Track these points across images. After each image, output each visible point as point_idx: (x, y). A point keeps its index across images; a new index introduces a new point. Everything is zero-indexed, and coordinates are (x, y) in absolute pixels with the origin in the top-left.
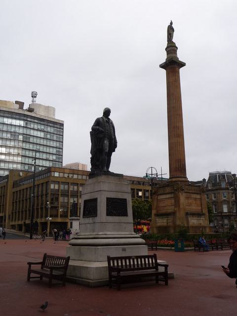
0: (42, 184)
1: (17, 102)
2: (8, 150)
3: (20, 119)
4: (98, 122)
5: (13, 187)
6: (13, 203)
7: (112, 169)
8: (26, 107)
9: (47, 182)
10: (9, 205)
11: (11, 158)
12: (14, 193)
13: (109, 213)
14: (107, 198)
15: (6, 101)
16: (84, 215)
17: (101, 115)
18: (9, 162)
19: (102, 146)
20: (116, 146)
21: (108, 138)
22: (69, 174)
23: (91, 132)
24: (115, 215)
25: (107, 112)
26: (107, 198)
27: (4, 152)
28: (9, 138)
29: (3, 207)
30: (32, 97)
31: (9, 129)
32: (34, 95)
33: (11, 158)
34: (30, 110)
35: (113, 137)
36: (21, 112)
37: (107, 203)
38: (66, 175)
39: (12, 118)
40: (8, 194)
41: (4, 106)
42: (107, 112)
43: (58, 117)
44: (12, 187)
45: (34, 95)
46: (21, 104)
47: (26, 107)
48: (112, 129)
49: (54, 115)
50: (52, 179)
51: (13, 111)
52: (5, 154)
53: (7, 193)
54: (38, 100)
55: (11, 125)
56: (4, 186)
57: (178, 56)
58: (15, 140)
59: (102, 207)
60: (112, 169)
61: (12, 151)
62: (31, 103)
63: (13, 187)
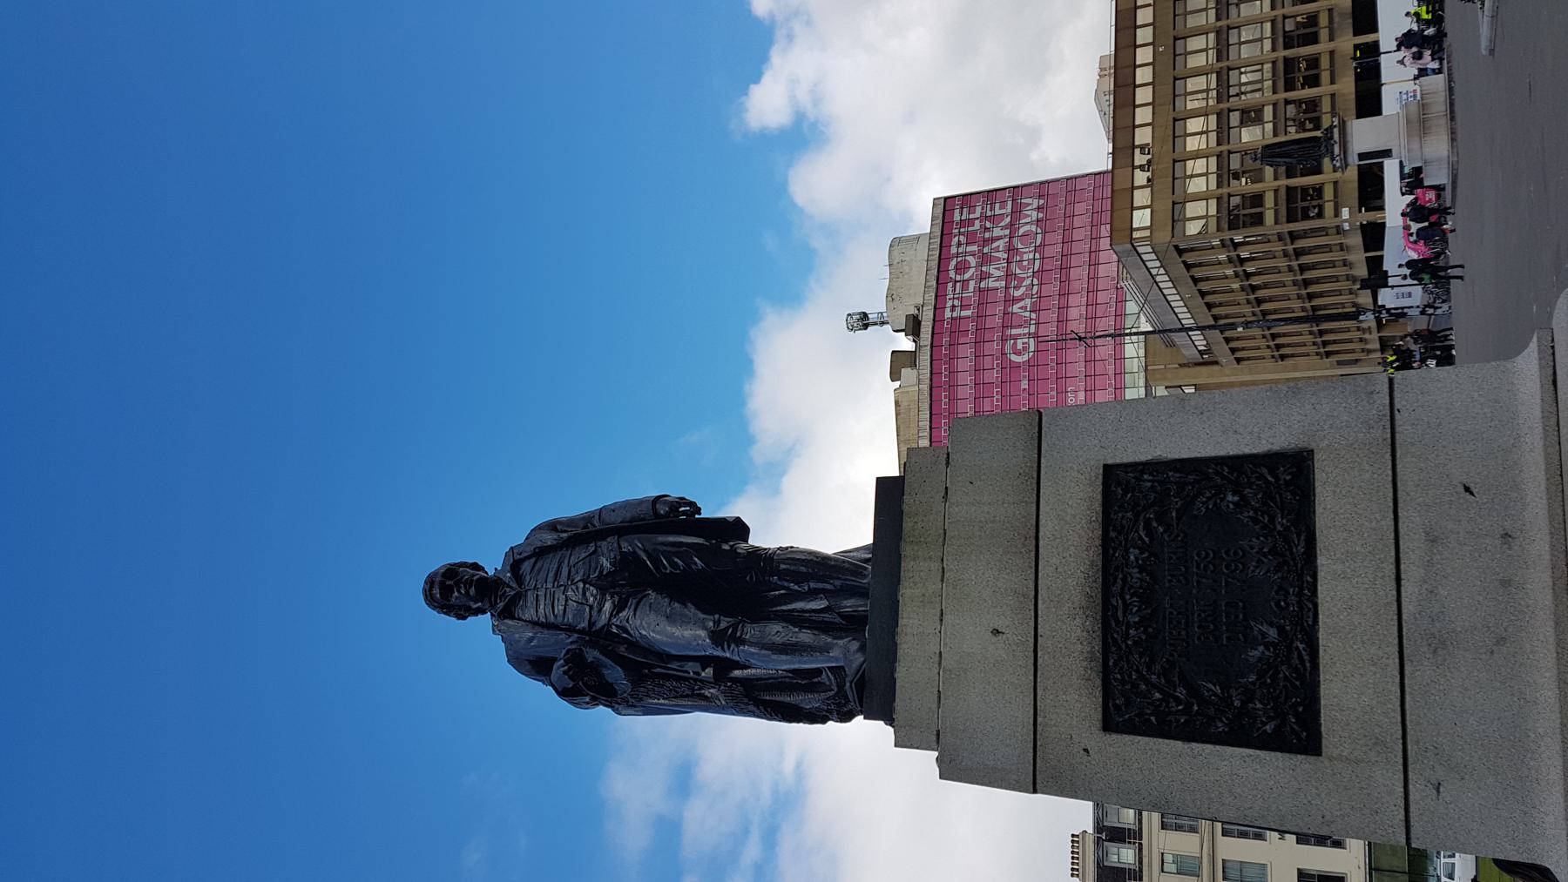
0: (1188, 267)
1: (895, 375)
8: (906, 343)
9: (1180, 252)
10: (1295, 369)
12: (1238, 360)
16: (1290, 190)
22: (1134, 167)
30: (866, 326)
32: (864, 321)
34: (913, 327)
38: (1141, 178)
39: (952, 386)
43: (922, 221)
44: (1216, 368)
45: (864, 321)
46: (900, 361)
47: (906, 343)
49: (918, 237)
50: (1164, 236)
51: (925, 387)
52: (1093, 278)
54: (876, 305)
57: (830, 723)
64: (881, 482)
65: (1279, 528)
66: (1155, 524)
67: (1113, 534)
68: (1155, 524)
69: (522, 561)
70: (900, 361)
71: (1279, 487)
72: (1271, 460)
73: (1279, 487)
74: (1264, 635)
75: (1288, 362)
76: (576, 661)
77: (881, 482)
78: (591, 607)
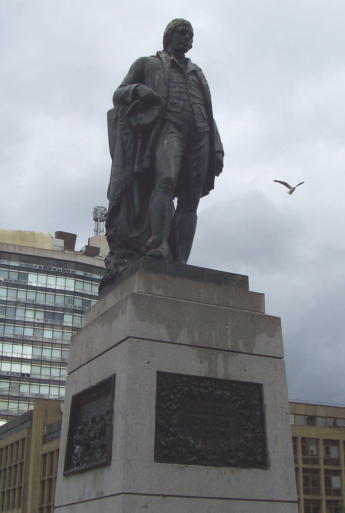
1: (60, 235)
2: (38, 352)
3: (66, 275)
4: (141, 71)
5: (44, 442)
6: (43, 482)
7: (196, 258)
8: (80, 245)
11: (45, 373)
12: (44, 456)
13: (169, 449)
14: (159, 373)
15: (33, 233)
16: (68, 465)
17: (152, 45)
18: (40, 381)
19: (153, 159)
20: (216, 166)
21: (178, 128)
23: (110, 113)
24: (201, 460)
25: (179, 36)
26: (159, 373)
27: (30, 357)
28: (42, 321)
29: (20, 494)
31: (41, 298)
33: (45, 373)
35: (202, 125)
36: (67, 256)
37: (159, 398)
39: (47, 272)
40: (32, 459)
41: (31, 244)
42: (179, 36)
46: (69, 239)
47: (80, 245)
48: (196, 92)
53: (28, 457)
55: (46, 290)
56: (23, 440)
58: (52, 326)
59: (134, 421)
60: (196, 258)
61: (47, 353)
62: (92, 234)
63: (44, 442)
64: (245, 279)
65: (239, 454)
66: (239, 403)
67: (235, 385)
68: (239, 403)
69: (196, 75)
70: (69, 239)
71: (253, 455)
72: (265, 453)
73: (253, 455)
74: (197, 443)
75: (39, 485)
76: (150, 102)
77: (245, 279)
78: (178, 113)
